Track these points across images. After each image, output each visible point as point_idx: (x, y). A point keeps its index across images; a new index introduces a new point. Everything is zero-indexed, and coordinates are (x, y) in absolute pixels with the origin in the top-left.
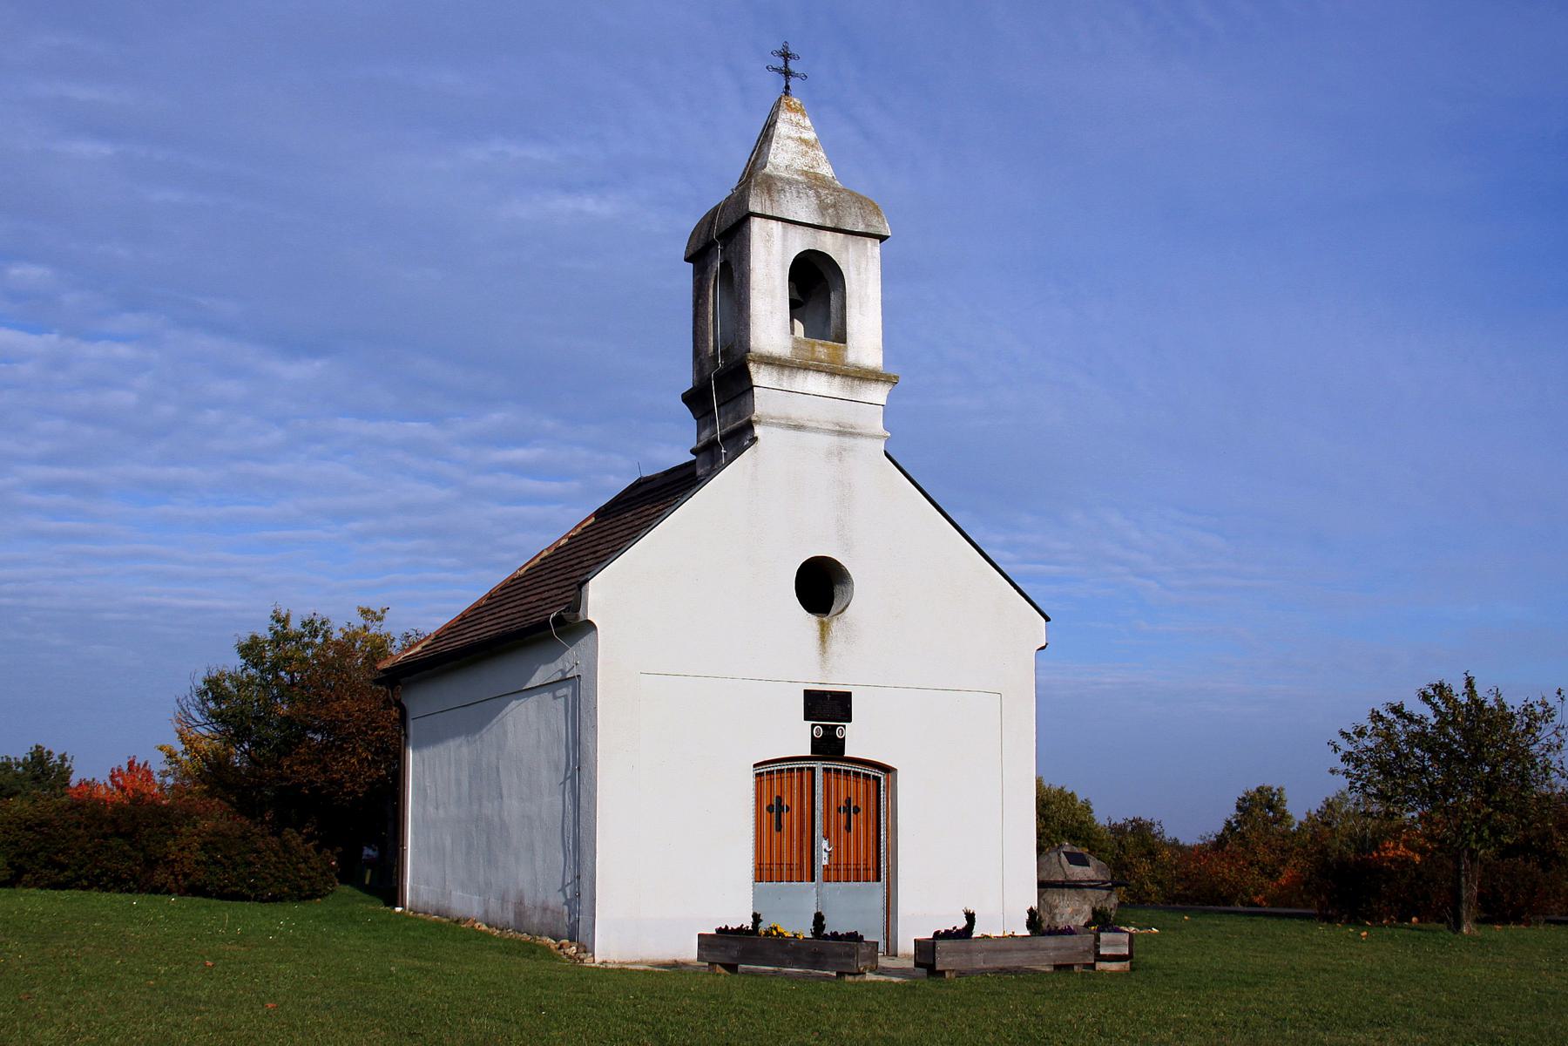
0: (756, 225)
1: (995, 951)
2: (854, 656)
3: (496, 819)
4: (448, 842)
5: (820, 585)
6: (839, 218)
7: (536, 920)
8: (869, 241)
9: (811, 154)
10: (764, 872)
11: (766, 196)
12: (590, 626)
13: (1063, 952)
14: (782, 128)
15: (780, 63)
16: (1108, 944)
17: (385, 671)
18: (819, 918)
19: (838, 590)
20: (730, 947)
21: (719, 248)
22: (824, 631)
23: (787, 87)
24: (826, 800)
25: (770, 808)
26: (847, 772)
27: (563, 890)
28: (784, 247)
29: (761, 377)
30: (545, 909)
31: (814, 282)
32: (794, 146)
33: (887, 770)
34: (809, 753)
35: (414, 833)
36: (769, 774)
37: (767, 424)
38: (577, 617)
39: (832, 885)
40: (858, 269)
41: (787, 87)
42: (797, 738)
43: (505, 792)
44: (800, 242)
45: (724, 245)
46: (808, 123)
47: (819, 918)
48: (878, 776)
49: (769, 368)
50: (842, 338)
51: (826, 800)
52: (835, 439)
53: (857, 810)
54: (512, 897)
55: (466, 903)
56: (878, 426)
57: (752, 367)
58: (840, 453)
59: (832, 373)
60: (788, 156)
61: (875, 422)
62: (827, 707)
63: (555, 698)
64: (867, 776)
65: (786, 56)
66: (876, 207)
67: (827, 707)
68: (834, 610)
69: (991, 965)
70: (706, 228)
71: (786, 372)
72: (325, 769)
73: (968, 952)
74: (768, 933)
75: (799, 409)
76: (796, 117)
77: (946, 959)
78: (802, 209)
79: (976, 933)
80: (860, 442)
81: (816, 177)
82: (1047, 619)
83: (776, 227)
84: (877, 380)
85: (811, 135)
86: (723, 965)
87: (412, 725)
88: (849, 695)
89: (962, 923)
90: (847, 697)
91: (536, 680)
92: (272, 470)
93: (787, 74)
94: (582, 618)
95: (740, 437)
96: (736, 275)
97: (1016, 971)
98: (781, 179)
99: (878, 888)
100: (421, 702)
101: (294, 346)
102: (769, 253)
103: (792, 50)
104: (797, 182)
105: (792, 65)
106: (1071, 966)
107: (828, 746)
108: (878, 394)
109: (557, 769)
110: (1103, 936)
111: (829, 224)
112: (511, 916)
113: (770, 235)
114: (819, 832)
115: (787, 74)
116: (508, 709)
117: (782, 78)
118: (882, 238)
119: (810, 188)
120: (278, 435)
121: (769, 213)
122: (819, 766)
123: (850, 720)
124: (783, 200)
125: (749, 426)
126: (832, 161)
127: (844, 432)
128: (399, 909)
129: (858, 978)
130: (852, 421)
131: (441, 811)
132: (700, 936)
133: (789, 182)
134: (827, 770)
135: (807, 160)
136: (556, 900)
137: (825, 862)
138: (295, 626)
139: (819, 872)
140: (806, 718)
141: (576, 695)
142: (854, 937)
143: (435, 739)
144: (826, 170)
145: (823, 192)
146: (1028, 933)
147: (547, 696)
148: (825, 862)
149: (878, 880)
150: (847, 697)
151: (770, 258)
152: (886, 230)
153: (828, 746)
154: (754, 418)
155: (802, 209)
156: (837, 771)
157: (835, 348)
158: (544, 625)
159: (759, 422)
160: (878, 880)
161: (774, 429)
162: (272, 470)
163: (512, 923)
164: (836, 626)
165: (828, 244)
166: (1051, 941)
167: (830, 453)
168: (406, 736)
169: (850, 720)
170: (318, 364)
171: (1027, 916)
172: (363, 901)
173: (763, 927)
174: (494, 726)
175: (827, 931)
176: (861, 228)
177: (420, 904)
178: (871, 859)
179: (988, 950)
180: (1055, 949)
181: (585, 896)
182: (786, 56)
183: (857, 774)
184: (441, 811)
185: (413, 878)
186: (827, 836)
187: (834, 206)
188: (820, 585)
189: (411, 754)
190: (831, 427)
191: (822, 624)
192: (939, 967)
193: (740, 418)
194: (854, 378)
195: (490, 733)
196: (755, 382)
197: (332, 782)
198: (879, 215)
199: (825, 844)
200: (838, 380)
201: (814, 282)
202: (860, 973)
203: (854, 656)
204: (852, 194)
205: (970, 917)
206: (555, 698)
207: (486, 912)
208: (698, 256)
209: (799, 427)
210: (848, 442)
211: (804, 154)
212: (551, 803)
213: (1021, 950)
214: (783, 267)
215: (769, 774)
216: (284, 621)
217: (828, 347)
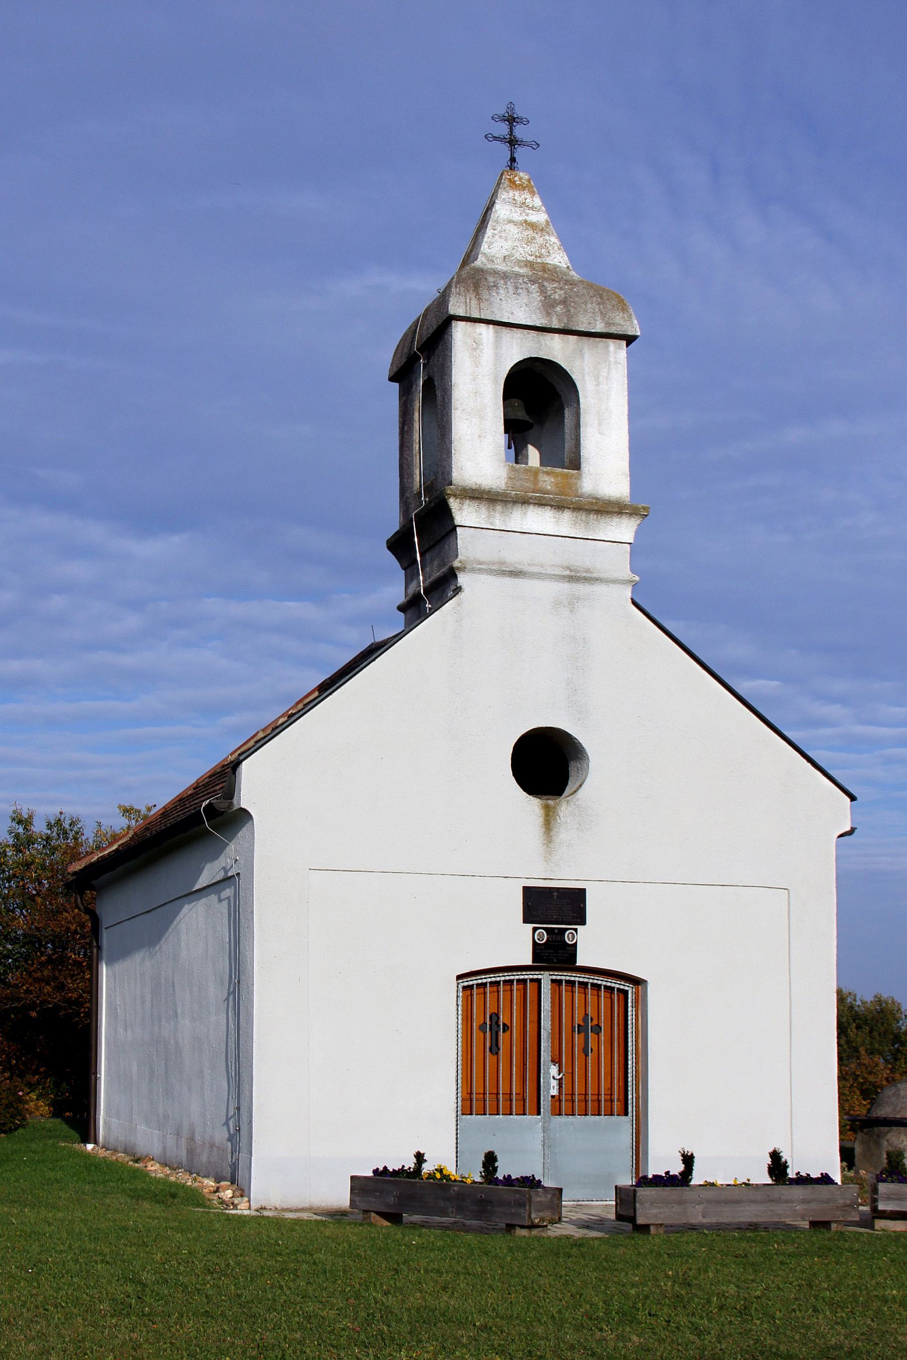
0: (460, 332)
1: (719, 1202)
2: (585, 845)
3: (172, 1041)
4: (135, 1069)
5: (545, 763)
6: (570, 316)
7: (204, 1158)
8: (612, 344)
9: (540, 240)
10: (475, 1100)
11: (473, 295)
12: (244, 816)
13: (814, 1206)
14: (501, 210)
15: (502, 129)
16: (889, 1198)
17: (75, 873)
18: (490, 1160)
19: (573, 767)
20: (394, 1194)
21: (422, 364)
22: (549, 820)
23: (513, 160)
24: (553, 1014)
25: (482, 1028)
26: (583, 985)
27: (227, 1124)
28: (497, 356)
29: (465, 514)
30: (212, 1146)
31: (538, 401)
32: (517, 231)
33: (637, 982)
34: (529, 962)
35: (107, 1058)
36: (477, 987)
37: (473, 570)
38: (231, 804)
39: (563, 1119)
40: (597, 377)
41: (513, 160)
42: (515, 944)
43: (179, 1011)
44: (518, 347)
45: (428, 358)
46: (537, 201)
47: (490, 1160)
48: (622, 993)
49: (475, 504)
50: (576, 464)
51: (553, 1014)
52: (566, 587)
53: (597, 1029)
54: (185, 1133)
55: (149, 1139)
56: (625, 572)
57: (453, 503)
58: (573, 603)
59: (560, 507)
60: (508, 245)
61: (619, 563)
62: (555, 910)
63: (220, 900)
64: (609, 989)
65: (512, 120)
66: (621, 301)
67: (555, 910)
68: (568, 791)
69: (714, 1220)
70: (409, 339)
71: (499, 508)
72: (61, 987)
73: (681, 1203)
74: (431, 1176)
75: (516, 552)
76: (519, 196)
77: (652, 1208)
78: (520, 307)
79: (697, 1179)
80: (599, 589)
81: (544, 268)
82: (853, 798)
83: (486, 332)
84: (620, 513)
85: (541, 217)
86: (377, 1213)
87: (105, 936)
88: (582, 892)
89: (677, 1168)
90: (580, 894)
91: (202, 882)
92: (128, 660)
93: (513, 142)
94: (236, 807)
95: (443, 587)
96: (439, 393)
97: (754, 1227)
98: (495, 273)
99: (624, 1125)
100: (115, 907)
101: (150, 519)
102: (477, 364)
103: (519, 112)
104: (517, 275)
105: (520, 132)
106: (826, 1225)
107: (555, 953)
108: (624, 530)
109: (222, 982)
110: (882, 1187)
111: (555, 324)
112: (183, 1154)
113: (477, 343)
114: (545, 1056)
115: (513, 142)
116: (181, 915)
117: (505, 149)
118: (630, 340)
119: (533, 282)
120: (133, 621)
121: (476, 315)
122: (546, 978)
123: (583, 922)
124: (495, 298)
125: (451, 575)
126: (567, 246)
127: (575, 577)
128: (90, 1147)
129: (535, 1232)
130: (588, 563)
131: (129, 1033)
132: (353, 1178)
133: (505, 276)
134: (556, 983)
135: (533, 248)
136: (221, 1136)
137: (554, 1092)
138: (39, 827)
139: (545, 1103)
140: (526, 921)
141: (236, 895)
142: (530, 1182)
143: (123, 953)
144: (559, 259)
145: (549, 286)
146: (769, 1181)
147: (213, 898)
148: (554, 1092)
149: (626, 1114)
150: (580, 894)
151: (478, 372)
152: (634, 328)
153: (555, 953)
154: (456, 564)
155: (520, 307)
156: (571, 983)
157: (566, 476)
158: (195, 818)
159: (463, 569)
160: (626, 1114)
161: (483, 577)
162: (128, 660)
163: (184, 1160)
164: (565, 808)
165: (555, 349)
166: (798, 1192)
167: (557, 604)
168: (99, 948)
169: (583, 922)
170: (176, 539)
171: (769, 1161)
172: (66, 1138)
173: (427, 1168)
174: (170, 934)
175: (500, 1175)
176: (599, 327)
177: (112, 1141)
178: (612, 1085)
179: (709, 1202)
180: (804, 1201)
181: (244, 1131)
182: (512, 120)
183: (597, 987)
184: (129, 1033)
185: (106, 1111)
186: (556, 1060)
187: (564, 302)
188: (545, 763)
189: (104, 970)
190: (558, 571)
191: (547, 808)
192: (640, 1221)
193: (444, 564)
194: (589, 511)
195: (166, 945)
196: (458, 520)
197: (70, 1002)
198: (624, 310)
199: (554, 1070)
200: (567, 515)
201: (538, 401)
202: (532, 1226)
203: (585, 845)
204: (590, 286)
205: (688, 1160)
206: (220, 900)
207: (164, 1148)
208: (402, 374)
209: (516, 574)
210: (582, 589)
211: (530, 241)
212: (216, 1022)
213: (754, 1202)
214: (496, 381)
215: (477, 987)
216: (24, 821)
217: (556, 475)
